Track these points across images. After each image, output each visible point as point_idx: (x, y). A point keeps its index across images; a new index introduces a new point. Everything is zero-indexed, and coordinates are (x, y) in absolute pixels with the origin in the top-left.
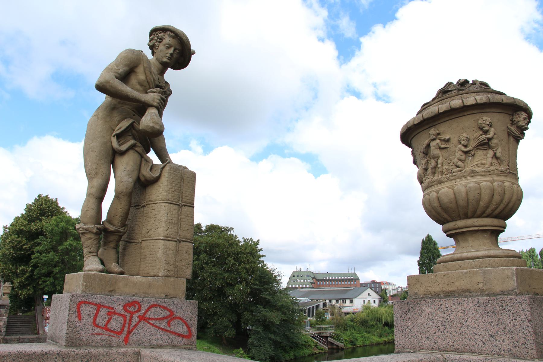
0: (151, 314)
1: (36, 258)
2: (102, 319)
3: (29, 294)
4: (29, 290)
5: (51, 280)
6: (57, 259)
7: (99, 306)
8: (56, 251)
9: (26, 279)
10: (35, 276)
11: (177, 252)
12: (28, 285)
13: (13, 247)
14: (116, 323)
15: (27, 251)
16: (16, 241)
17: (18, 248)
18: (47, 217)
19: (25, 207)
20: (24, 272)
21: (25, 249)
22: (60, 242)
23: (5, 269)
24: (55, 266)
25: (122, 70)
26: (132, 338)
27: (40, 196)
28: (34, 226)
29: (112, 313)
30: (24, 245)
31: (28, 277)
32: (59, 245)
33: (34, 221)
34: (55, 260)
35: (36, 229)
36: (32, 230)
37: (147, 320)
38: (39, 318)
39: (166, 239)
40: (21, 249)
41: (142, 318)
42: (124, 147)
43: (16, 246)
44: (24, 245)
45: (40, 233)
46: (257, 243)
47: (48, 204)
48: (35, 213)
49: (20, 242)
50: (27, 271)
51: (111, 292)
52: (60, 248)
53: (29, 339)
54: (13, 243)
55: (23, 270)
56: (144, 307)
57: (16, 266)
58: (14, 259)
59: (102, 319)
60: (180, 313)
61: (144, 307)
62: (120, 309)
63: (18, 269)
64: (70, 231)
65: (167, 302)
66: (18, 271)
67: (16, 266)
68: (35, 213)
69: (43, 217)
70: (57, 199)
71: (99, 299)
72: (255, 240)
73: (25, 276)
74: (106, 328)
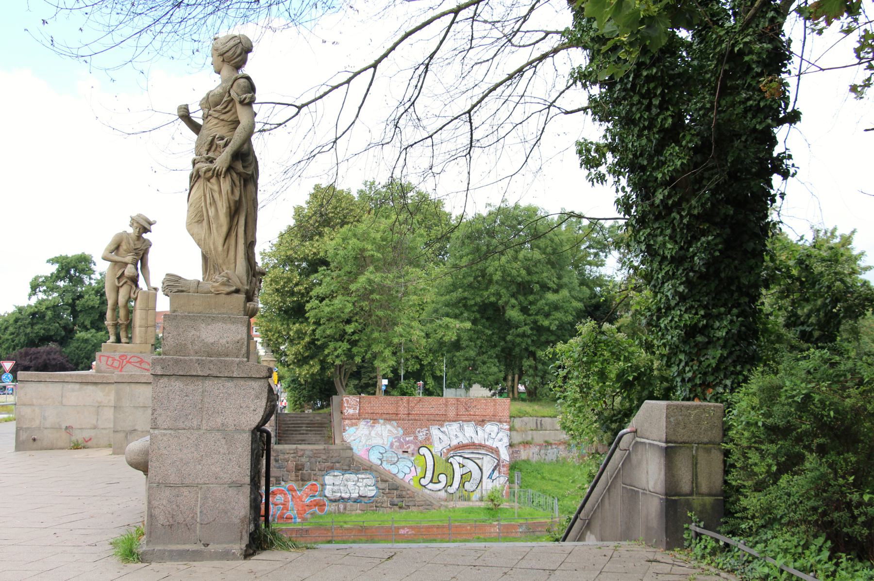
0: (132, 360)
1: (312, 309)
2: (110, 362)
3: (313, 374)
4: (312, 366)
5: (345, 345)
6: (349, 307)
7: (108, 357)
8: (347, 291)
9: (307, 347)
10: (318, 340)
11: (146, 332)
12: (312, 357)
13: (277, 290)
14: (116, 364)
15: (303, 295)
16: (282, 278)
17: (287, 292)
18: (333, 227)
19: (292, 213)
20: (300, 335)
21: (299, 292)
22: (353, 277)
23: (270, 331)
24: (348, 322)
25: (113, 248)
26: (124, 370)
27: (317, 187)
28: (309, 248)
29: (114, 360)
30: (297, 285)
31: (309, 343)
32: (352, 282)
33: (311, 239)
34: (347, 310)
35: (314, 254)
36: (308, 255)
37: (130, 363)
38: (336, 417)
39: (140, 327)
40: (292, 294)
41: (128, 362)
42: (121, 284)
43: (284, 287)
44: (297, 285)
45: (317, 264)
46: (847, 241)
47: (334, 201)
48: (311, 222)
49: (289, 280)
50: (305, 334)
51: (115, 351)
52: (353, 287)
53: (312, 450)
54: (277, 283)
55: (299, 332)
56: (129, 357)
57: (288, 325)
58: (286, 312)
59: (110, 362)
60: (146, 360)
61: (129, 357)
62: (117, 358)
63: (290, 329)
64: (367, 254)
65: (140, 355)
66: (291, 333)
67: (288, 325)
68: (311, 222)
69: (326, 229)
70: (349, 189)
71: (108, 354)
72: (843, 230)
73: (303, 343)
74: (111, 366)
